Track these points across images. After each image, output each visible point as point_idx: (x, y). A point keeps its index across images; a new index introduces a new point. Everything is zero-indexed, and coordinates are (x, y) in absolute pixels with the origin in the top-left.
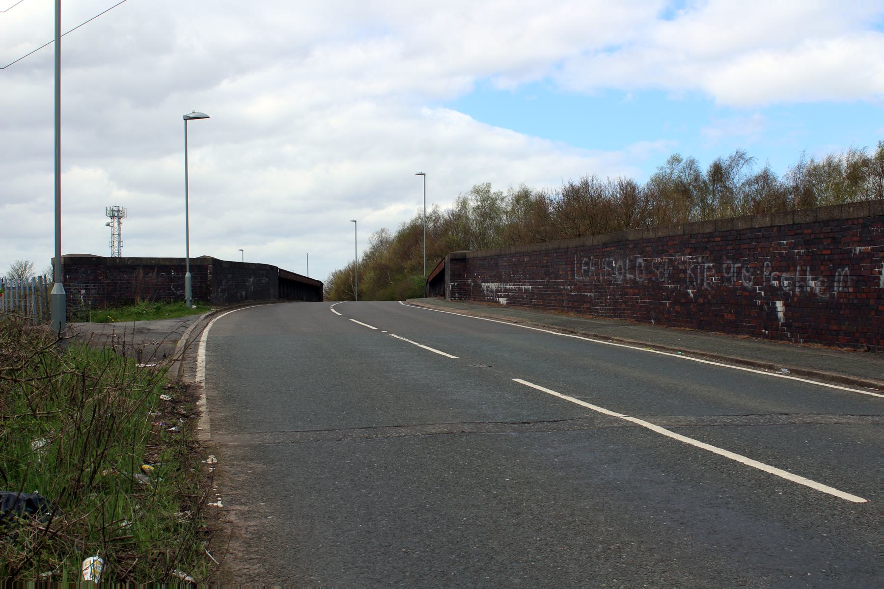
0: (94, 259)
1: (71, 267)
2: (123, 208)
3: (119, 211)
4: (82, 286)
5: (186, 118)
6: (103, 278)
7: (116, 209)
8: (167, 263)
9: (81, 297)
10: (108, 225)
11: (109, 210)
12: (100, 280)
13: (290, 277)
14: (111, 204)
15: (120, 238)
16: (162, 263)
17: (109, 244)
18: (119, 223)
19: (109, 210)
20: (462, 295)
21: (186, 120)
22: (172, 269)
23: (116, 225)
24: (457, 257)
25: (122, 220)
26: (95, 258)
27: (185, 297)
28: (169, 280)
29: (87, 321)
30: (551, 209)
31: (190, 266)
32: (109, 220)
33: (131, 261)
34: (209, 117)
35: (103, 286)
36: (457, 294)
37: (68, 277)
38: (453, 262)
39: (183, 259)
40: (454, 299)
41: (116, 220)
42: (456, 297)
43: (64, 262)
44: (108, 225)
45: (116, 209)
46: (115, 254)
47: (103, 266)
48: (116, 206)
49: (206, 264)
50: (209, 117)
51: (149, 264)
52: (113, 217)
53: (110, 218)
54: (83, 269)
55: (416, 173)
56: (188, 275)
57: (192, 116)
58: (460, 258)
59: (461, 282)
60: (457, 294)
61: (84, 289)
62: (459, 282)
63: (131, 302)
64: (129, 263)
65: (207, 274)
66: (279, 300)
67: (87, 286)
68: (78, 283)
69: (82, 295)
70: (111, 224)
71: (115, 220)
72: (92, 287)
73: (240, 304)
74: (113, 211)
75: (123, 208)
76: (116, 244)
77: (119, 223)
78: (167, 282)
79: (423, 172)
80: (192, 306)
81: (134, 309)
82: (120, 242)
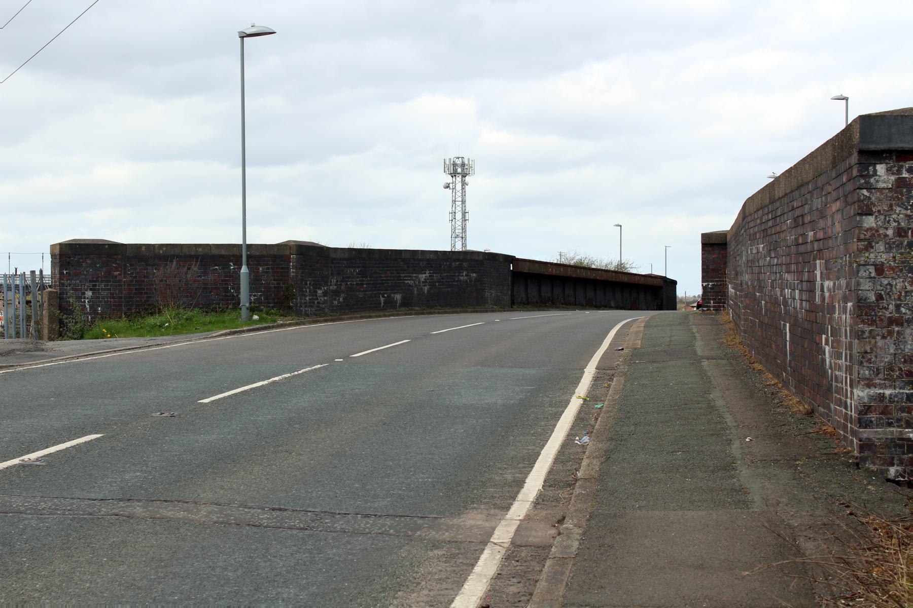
0: (107, 247)
1: (70, 258)
2: (469, 159)
3: (463, 165)
4: (87, 286)
5: (243, 36)
6: (119, 275)
7: (459, 162)
8: (223, 252)
9: (85, 301)
10: (447, 187)
11: (447, 162)
12: (116, 277)
13: (535, 270)
14: (452, 155)
15: (465, 206)
16: (215, 252)
17: (448, 217)
18: (464, 184)
19: (447, 162)
20: (720, 303)
21: (242, 37)
22: (232, 261)
23: (459, 186)
24: (711, 242)
25: (467, 179)
26: (108, 245)
27: (240, 303)
28: (226, 276)
29: (82, 337)
30: (894, 157)
31: (248, 257)
32: (449, 179)
33: (164, 249)
34: (275, 33)
35: (120, 286)
36: (712, 302)
37: (65, 272)
38: (707, 249)
39: (238, 246)
40: (708, 310)
41: (459, 179)
42: (710, 307)
43: (60, 251)
44: (447, 187)
45: (459, 162)
46: (457, 231)
47: (120, 257)
48: (458, 158)
49: (288, 252)
50: (275, 33)
51: (193, 254)
52: (454, 174)
53: (450, 176)
54: (89, 261)
55: (831, 98)
56: (244, 269)
57: (248, 32)
58: (716, 242)
59: (716, 281)
60: (712, 302)
61: (91, 289)
62: (716, 281)
63: (153, 310)
64: (161, 252)
65: (289, 269)
66: (512, 307)
67: (95, 286)
68: (81, 282)
69: (88, 298)
70: (451, 186)
71: (458, 179)
72: (103, 286)
73: (432, 311)
74: (455, 165)
75: (469, 159)
76: (459, 216)
77: (464, 184)
78: (222, 281)
79: (845, 95)
80: (252, 316)
81: (151, 320)
82: (464, 213)
